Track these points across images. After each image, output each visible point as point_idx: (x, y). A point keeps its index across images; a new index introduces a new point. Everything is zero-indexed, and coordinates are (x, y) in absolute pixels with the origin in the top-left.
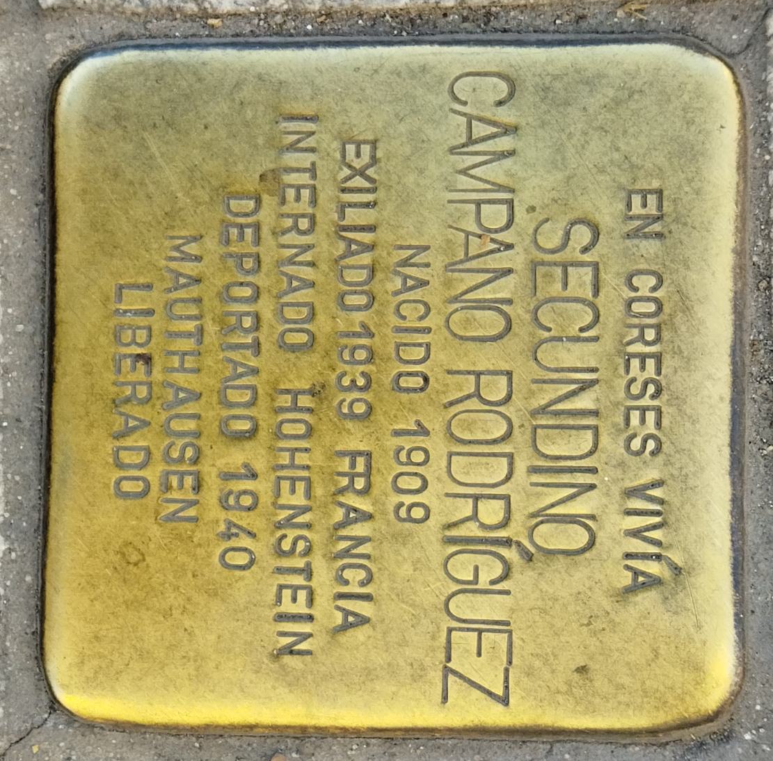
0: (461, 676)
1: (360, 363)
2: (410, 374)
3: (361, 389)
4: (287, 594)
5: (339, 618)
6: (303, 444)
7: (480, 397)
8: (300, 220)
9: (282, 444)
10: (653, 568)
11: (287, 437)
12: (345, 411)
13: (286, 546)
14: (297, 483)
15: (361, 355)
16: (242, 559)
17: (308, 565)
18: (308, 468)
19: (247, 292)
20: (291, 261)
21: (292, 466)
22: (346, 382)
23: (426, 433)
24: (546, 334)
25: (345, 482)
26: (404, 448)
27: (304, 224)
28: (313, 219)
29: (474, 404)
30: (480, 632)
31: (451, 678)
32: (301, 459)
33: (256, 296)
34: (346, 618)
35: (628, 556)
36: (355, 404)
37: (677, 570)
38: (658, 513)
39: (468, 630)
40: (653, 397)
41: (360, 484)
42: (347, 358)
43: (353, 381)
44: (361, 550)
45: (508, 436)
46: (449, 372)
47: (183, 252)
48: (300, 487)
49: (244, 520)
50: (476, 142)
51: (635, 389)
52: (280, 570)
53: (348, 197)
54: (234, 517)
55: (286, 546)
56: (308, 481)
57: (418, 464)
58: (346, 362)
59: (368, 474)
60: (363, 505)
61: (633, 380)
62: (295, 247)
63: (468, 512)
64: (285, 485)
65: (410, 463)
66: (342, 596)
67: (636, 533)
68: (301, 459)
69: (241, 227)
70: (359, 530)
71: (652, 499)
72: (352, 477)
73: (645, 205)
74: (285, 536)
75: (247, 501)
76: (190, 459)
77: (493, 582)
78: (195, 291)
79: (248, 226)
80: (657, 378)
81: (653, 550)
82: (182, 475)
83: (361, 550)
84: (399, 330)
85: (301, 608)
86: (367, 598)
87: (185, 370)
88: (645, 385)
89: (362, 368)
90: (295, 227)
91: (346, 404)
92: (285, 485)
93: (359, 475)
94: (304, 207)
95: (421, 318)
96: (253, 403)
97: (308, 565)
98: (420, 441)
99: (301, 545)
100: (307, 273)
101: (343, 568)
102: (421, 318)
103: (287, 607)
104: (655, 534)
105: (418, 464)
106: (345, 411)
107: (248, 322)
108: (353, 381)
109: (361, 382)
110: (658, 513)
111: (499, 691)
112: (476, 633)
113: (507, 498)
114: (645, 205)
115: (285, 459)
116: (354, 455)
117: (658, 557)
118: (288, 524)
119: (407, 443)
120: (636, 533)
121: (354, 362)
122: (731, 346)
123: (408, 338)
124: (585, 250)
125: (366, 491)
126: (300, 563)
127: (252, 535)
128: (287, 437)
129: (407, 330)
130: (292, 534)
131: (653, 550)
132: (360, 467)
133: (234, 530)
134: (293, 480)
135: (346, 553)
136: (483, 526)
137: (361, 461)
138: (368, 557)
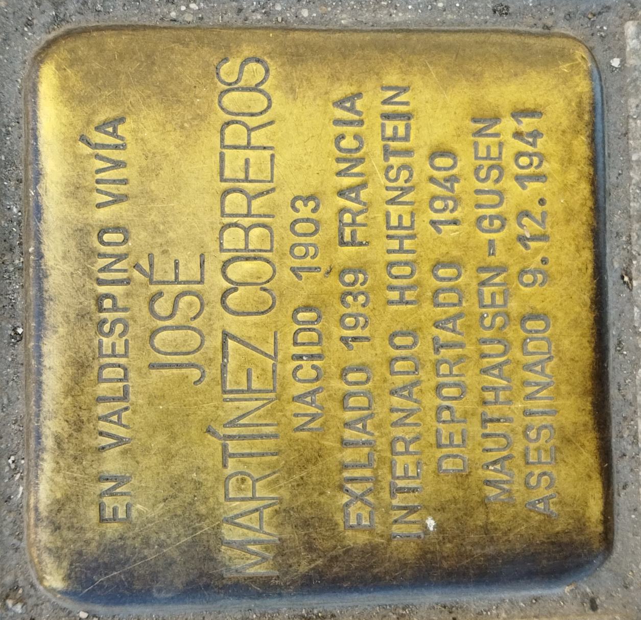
0: (266, 355)
1: (350, 315)
2: (305, 235)
3: (350, 294)
4: (401, 132)
5: (359, 104)
6: (394, 257)
7: (246, 194)
8: (350, 221)
9: (410, 257)
10: (99, 138)
11: (406, 263)
12: (361, 276)
13: (404, 174)
14: (396, 224)
15: (349, 321)
16: (440, 162)
17: (386, 159)
18: (389, 237)
19: (445, 392)
20: (410, 413)
21: (401, 239)
22: (361, 298)
23: (293, 269)
24: (264, 286)
25: (359, 219)
26: (311, 257)
27: (400, 447)
28: (393, 452)
29: (253, 122)
30: (246, 249)
31: (270, 351)
32: (395, 244)
33: (439, 388)
34: (353, 104)
35: (116, 147)
36: (352, 325)
37: (84, 139)
38: (98, 182)
39: (260, 391)
40: (104, 321)
41: (347, 218)
42: (361, 319)
43: (355, 299)
44: (343, 166)
45: (225, 264)
46: (275, 333)
47: (501, 489)
48: (394, 222)
49: (438, 190)
50: (257, 510)
51: (119, 328)
52: (408, 152)
53: (367, 473)
54: (530, 149)
55: (404, 174)
56: (389, 227)
57: (300, 245)
58: (361, 315)
59: (342, 225)
60: (342, 202)
61: (122, 335)
62: (402, 411)
63: (253, 134)
64: (406, 222)
65: (306, 246)
66: (361, 123)
67: (118, 164)
68: (395, 244)
69: (451, 445)
70: (347, 181)
71: (102, 158)
72: (354, 223)
73: (395, 128)
74: (406, 181)
75: (438, 204)
76: (483, 168)
77: (235, 290)
78: (486, 362)
79: (446, 446)
80: (101, 337)
81: (102, 152)
82: (488, 157)
83: (343, 166)
84: (320, 357)
85: (390, 125)
86: (338, 122)
87: (494, 389)
88: (112, 331)
89: (349, 311)
90: (407, 443)
91: (361, 280)
92: (406, 222)
93: (349, 225)
94: (400, 461)
95: (300, 367)
96: (436, 293)
97: (386, 159)
98: (297, 263)
99: (392, 174)
100: (396, 401)
101: (358, 149)
102: (300, 367)
103: (401, 126)
104: (101, 164)
105: (300, 245)
106: (361, 276)
107: (444, 369)
108: (355, 299)
109: (350, 299)
110: (98, 182)
111: (230, 343)
112: (257, 496)
113: (223, 180)
114: (395, 128)
115: (407, 244)
116: (353, 243)
117: (96, 146)
118: (404, 191)
119: (308, 262)
120: (118, 164)
121: (355, 316)
122: (40, 154)
123: (315, 350)
124: (160, 294)
125: (343, 211)
126: (394, 161)
127: (432, 180)
128: (406, 263)
129: (312, 357)
130: (401, 183)
131: (102, 152)
132: (347, 231)
133: (448, 185)
134: (400, 227)
135: (361, 160)
136: (241, 191)
137: (347, 238)
138: (338, 160)
